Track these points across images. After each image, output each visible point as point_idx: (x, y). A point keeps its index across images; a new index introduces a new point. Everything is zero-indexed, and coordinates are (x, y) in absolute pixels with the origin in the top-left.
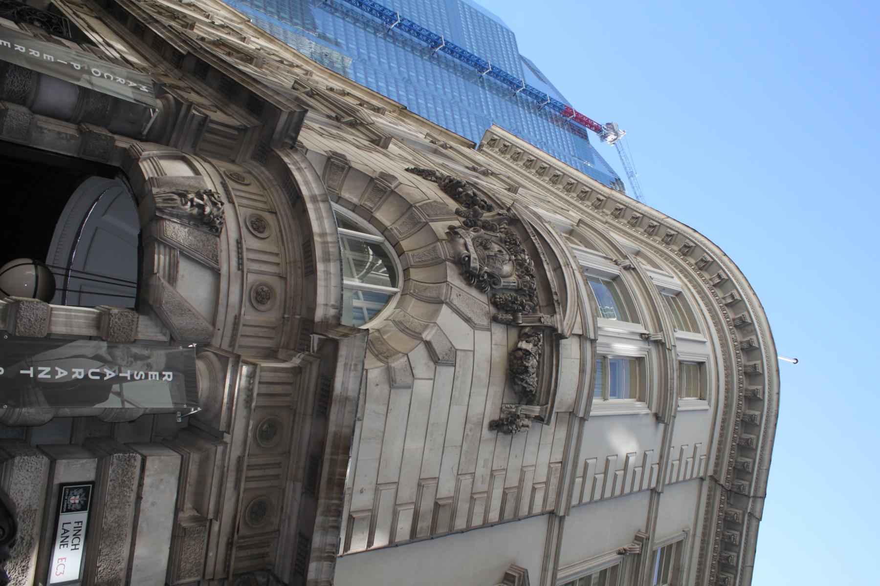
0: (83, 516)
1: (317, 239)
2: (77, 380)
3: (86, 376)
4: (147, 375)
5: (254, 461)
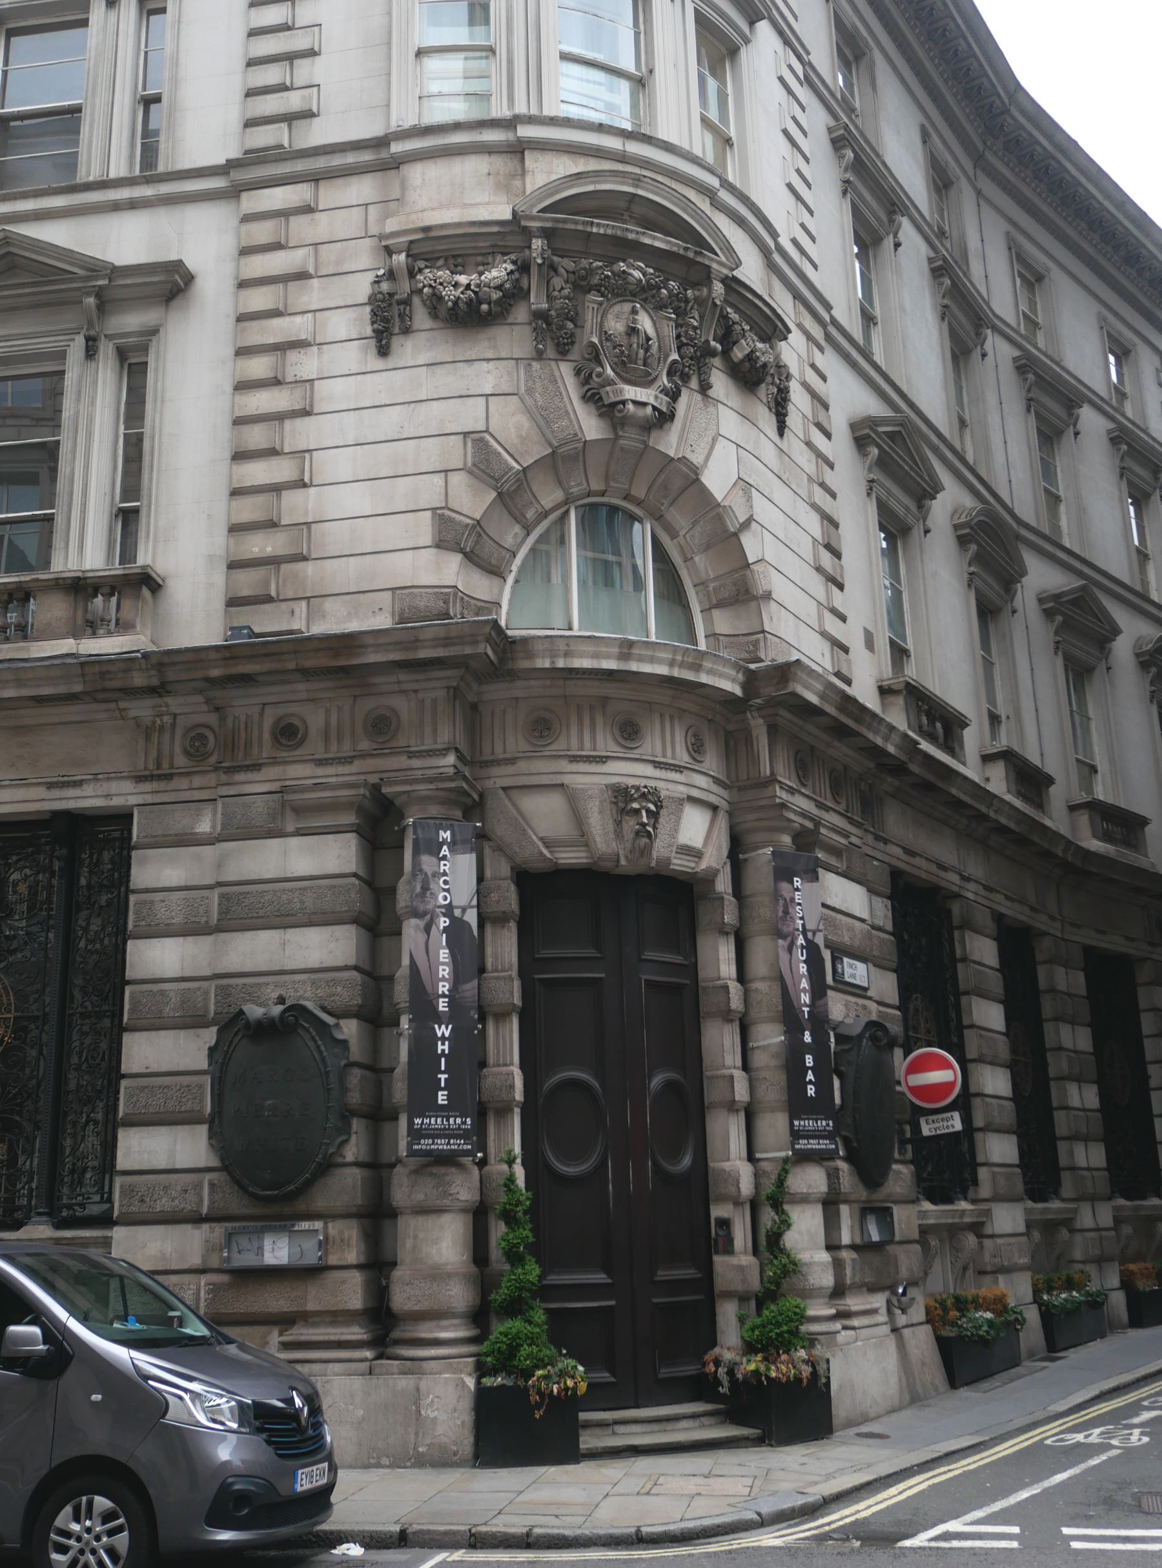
1: (676, 673)
2: (808, 970)
3: (805, 962)
4: (799, 904)
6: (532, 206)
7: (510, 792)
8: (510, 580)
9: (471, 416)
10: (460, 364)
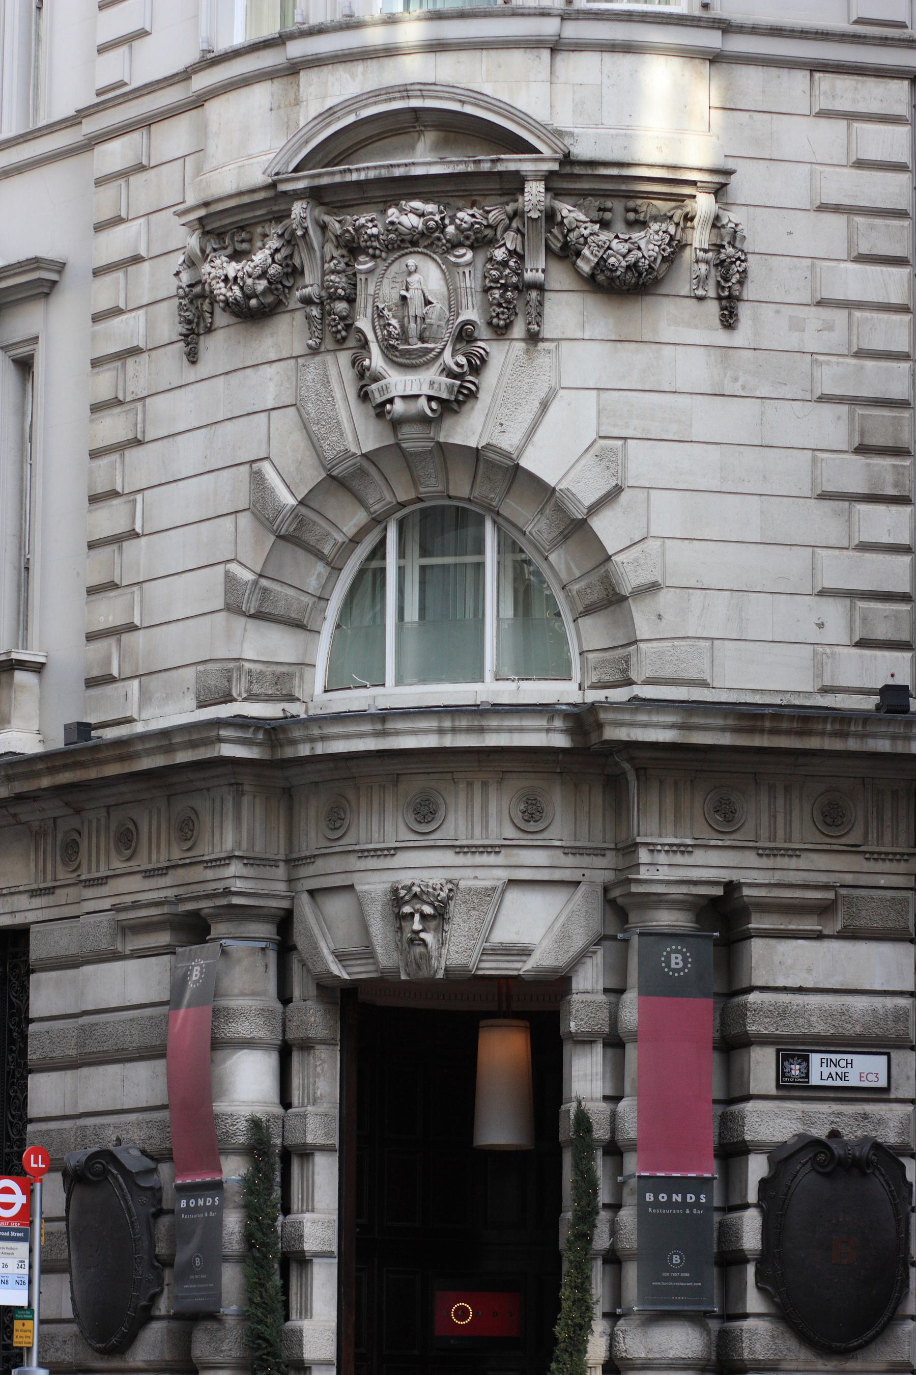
0: (815, 1059)
5: (764, 832)
6: (288, 163)
7: (320, 898)
8: (327, 629)
9: (247, 439)
10: (248, 371)
